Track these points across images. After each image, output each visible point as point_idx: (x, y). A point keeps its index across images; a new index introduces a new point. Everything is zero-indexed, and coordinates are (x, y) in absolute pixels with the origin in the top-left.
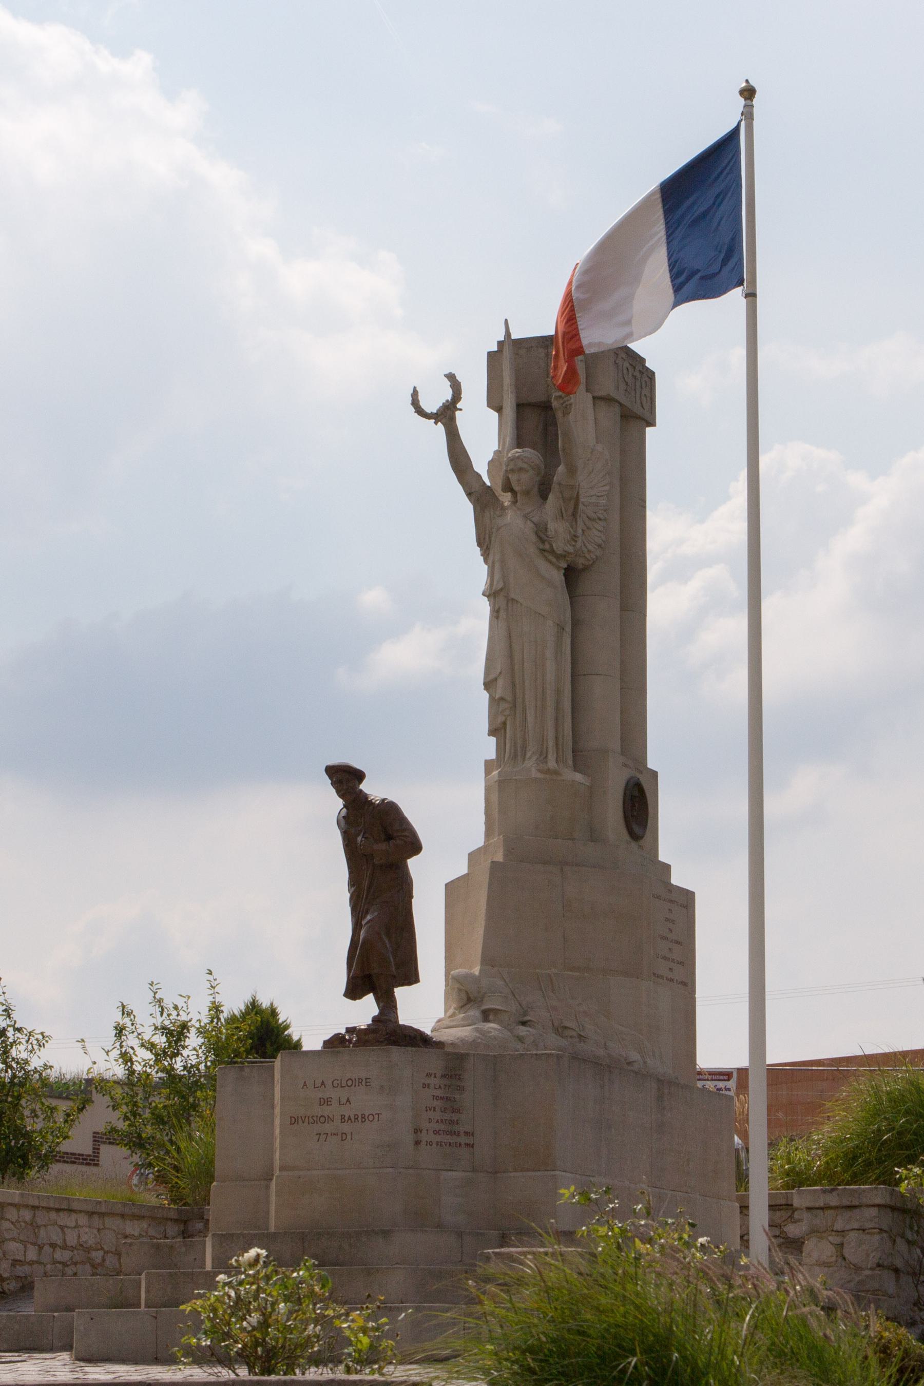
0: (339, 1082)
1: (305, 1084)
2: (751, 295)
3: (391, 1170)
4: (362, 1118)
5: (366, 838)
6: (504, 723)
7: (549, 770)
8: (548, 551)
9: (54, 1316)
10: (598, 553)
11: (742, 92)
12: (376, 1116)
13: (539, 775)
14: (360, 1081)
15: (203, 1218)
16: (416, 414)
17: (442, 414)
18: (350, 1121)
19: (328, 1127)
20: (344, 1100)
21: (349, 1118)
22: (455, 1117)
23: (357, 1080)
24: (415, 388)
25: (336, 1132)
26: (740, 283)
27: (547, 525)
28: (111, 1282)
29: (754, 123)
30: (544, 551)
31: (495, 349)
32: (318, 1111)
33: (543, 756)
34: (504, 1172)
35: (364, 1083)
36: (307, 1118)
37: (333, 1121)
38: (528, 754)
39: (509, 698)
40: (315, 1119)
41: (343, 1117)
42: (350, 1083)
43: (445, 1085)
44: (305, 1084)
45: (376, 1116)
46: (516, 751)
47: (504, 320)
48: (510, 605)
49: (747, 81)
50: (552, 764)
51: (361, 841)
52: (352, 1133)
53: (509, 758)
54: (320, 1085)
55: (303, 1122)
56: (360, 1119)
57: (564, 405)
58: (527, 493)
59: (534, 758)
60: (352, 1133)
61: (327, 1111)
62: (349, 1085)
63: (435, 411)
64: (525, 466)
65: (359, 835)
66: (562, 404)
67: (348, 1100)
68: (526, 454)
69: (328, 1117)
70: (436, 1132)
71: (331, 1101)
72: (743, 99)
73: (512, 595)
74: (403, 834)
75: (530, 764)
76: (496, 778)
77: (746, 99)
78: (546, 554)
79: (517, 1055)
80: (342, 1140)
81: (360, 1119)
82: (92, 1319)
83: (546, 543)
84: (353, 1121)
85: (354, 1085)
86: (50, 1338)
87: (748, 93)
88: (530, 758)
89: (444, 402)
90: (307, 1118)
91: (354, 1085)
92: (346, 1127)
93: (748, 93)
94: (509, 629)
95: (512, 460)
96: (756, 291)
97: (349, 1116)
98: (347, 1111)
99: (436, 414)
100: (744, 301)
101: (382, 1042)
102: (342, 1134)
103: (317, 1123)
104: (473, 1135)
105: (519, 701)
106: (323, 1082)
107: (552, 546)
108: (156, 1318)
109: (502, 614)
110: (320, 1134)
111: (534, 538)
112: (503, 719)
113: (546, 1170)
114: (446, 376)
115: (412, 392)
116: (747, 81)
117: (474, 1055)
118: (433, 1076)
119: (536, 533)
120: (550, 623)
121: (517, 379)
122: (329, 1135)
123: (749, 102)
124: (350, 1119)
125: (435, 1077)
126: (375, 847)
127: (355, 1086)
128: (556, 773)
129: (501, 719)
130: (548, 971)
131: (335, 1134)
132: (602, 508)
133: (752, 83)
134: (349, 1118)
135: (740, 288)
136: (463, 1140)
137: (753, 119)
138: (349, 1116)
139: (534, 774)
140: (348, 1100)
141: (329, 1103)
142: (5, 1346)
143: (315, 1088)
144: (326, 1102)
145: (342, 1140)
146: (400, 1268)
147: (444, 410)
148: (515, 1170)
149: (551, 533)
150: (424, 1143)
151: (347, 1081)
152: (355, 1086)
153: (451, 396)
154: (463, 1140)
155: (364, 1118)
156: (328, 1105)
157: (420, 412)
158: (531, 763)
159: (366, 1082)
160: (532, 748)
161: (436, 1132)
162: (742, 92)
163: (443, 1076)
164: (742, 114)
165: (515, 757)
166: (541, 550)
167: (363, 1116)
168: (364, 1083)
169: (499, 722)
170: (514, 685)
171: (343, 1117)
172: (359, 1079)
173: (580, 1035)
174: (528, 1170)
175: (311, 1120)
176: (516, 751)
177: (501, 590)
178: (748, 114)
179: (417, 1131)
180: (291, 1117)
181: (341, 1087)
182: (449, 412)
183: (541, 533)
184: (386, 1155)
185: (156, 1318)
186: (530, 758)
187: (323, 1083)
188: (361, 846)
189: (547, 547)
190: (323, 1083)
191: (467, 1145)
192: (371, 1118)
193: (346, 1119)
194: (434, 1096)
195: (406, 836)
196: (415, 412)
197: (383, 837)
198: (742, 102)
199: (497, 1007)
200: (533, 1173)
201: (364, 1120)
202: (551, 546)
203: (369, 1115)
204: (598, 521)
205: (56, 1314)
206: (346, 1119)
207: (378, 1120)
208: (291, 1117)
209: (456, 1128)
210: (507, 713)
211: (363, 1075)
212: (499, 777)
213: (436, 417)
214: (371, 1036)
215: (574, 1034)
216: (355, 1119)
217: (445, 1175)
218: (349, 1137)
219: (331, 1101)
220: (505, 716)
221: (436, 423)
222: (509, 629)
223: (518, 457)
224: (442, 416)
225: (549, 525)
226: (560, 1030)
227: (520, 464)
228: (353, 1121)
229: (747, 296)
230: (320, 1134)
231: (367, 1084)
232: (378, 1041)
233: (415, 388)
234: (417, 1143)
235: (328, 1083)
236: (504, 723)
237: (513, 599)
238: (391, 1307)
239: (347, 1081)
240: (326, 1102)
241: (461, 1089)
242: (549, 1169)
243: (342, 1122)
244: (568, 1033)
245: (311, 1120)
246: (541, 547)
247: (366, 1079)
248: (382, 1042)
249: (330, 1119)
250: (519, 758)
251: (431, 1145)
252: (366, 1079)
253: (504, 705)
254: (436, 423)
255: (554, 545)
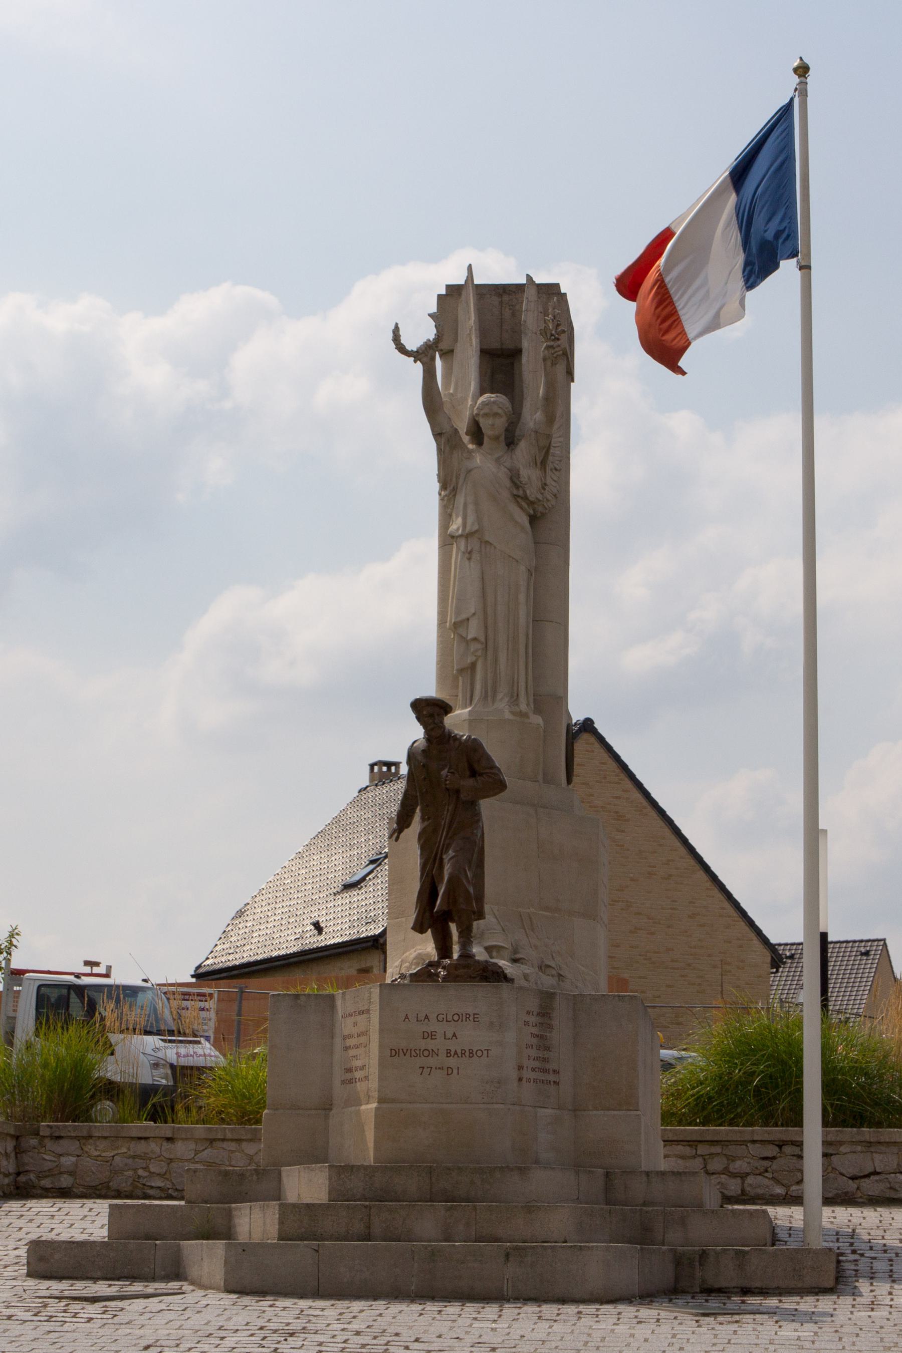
0: (445, 1017)
1: (407, 1017)
2: (805, 268)
3: (502, 1106)
4: (470, 1053)
5: (451, 773)
6: (473, 666)
7: (521, 712)
8: (522, 498)
9: (156, 1245)
10: (553, 502)
11: (795, 70)
12: (485, 1052)
13: (511, 717)
14: (468, 1016)
15: (38, 1134)
16: (397, 351)
17: (423, 352)
18: (456, 1056)
19: (432, 1061)
20: (449, 1035)
21: (456, 1053)
22: (546, 1054)
23: (464, 1015)
24: (397, 325)
25: (441, 1066)
26: (794, 254)
27: (519, 471)
28: (197, 1209)
29: (808, 98)
30: (519, 496)
31: (444, 292)
32: (423, 1044)
33: (514, 699)
34: (584, 1110)
35: (471, 1018)
36: (409, 1051)
37: (438, 1055)
38: (500, 696)
39: (483, 639)
40: (418, 1052)
41: (448, 1052)
42: (456, 1018)
43: (540, 1023)
44: (407, 1017)
45: (485, 1052)
46: (486, 692)
47: (468, 265)
48: (483, 547)
49: (801, 59)
50: (523, 707)
51: (447, 776)
52: (458, 1068)
53: (480, 699)
54: (423, 1018)
55: (405, 1055)
56: (467, 1054)
57: (555, 355)
58: (497, 438)
59: (507, 699)
60: (458, 1068)
61: (431, 1044)
62: (456, 1020)
63: (415, 349)
64: (500, 411)
65: (443, 769)
66: (553, 354)
67: (454, 1035)
68: (501, 400)
69: (433, 1050)
70: (533, 1070)
71: (435, 1035)
72: (797, 77)
73: (487, 538)
74: (491, 771)
75: (502, 704)
76: (466, 717)
77: (800, 76)
78: (519, 500)
79: (598, 995)
80: (448, 1074)
81: (467, 1054)
82: (244, 1250)
83: (520, 489)
84: (460, 1056)
85: (460, 1020)
86: (152, 1267)
87: (802, 70)
88: (501, 700)
89: (425, 341)
90: (409, 1051)
91: (460, 1020)
92: (452, 1062)
93: (802, 70)
94: (483, 570)
95: (487, 404)
96: (810, 263)
97: (456, 1051)
98: (453, 1046)
99: (417, 352)
100: (798, 273)
101: (474, 978)
102: (448, 1068)
103: (420, 1056)
104: (558, 1073)
105: (490, 644)
106: (426, 1015)
107: (526, 492)
108: (317, 1251)
109: (476, 556)
110: (423, 1068)
111: (508, 483)
112: (474, 659)
113: (628, 1110)
114: (429, 315)
115: (393, 328)
116: (801, 59)
117: (560, 993)
118: (531, 1014)
119: (511, 479)
120: (523, 568)
121: (480, 326)
122: (434, 1068)
123: (803, 79)
124: (457, 1054)
125: (533, 1014)
126: (462, 783)
127: (462, 1021)
128: (525, 715)
129: (470, 659)
130: (528, 911)
131: (439, 1068)
132: (557, 458)
133: (806, 60)
134: (456, 1053)
135: (795, 260)
136: (552, 1077)
137: (807, 96)
138: (456, 1051)
139: (508, 715)
140: (454, 1035)
141: (433, 1037)
142: (99, 1274)
143: (417, 1021)
144: (432, 1035)
145: (448, 1074)
146: (564, 1206)
147: (426, 349)
148: (596, 1109)
149: (524, 479)
150: (524, 1080)
151: (453, 1016)
152: (462, 1021)
153: (433, 337)
154: (552, 1077)
155: (471, 1053)
156: (431, 1039)
157: (401, 349)
158: (503, 705)
159: (474, 1018)
160: (503, 690)
161: (533, 1070)
162: (795, 70)
163: (538, 1014)
164: (796, 90)
165: (485, 697)
166: (515, 495)
167: (471, 1052)
168: (471, 1018)
169: (469, 661)
170: (486, 627)
171: (448, 1052)
172: (466, 1014)
173: (559, 974)
174: (609, 1110)
175: (413, 1053)
176: (486, 692)
177: (476, 532)
178: (802, 91)
179: (520, 1068)
180: (391, 1050)
181: (447, 1021)
182: (431, 352)
183: (514, 479)
184: (496, 1091)
185: (317, 1251)
186: (501, 700)
187: (426, 1017)
188: (446, 780)
189: (521, 493)
190: (426, 1017)
191: (555, 1082)
192: (479, 1053)
193: (452, 1053)
194: (532, 1033)
195: (494, 774)
196: (396, 348)
197: (468, 773)
198: (796, 79)
199: (502, 944)
200: (616, 1112)
201: (471, 1055)
202: (525, 491)
203: (477, 1051)
204: (554, 471)
205: (157, 1242)
206: (452, 1053)
207: (488, 1057)
208: (391, 1050)
209: (548, 1066)
210: (479, 653)
211: (470, 1010)
212: (469, 715)
213: (416, 355)
214: (461, 972)
215: (554, 972)
216: (462, 1054)
217: (542, 1112)
218: (455, 1071)
219: (435, 1035)
220: (475, 656)
221: (415, 361)
222: (483, 570)
223: (494, 402)
224: (423, 355)
225: (521, 471)
226: (543, 967)
227: (496, 409)
228: (460, 1056)
229: (801, 268)
230: (423, 1068)
231: (475, 1019)
232: (470, 977)
233: (397, 325)
234: (520, 1079)
235: (433, 1017)
236: (473, 666)
237: (487, 542)
238: (580, 1246)
239: (453, 1016)
240: (432, 1035)
241: (550, 1027)
242: (631, 1108)
243: (447, 1057)
244: (549, 971)
245: (413, 1053)
246: (515, 492)
247: (474, 1014)
248: (474, 978)
249: (433, 1053)
250: (489, 698)
251: (530, 1082)
252: (474, 1014)
253: (473, 647)
254: (415, 361)
255: (528, 492)
